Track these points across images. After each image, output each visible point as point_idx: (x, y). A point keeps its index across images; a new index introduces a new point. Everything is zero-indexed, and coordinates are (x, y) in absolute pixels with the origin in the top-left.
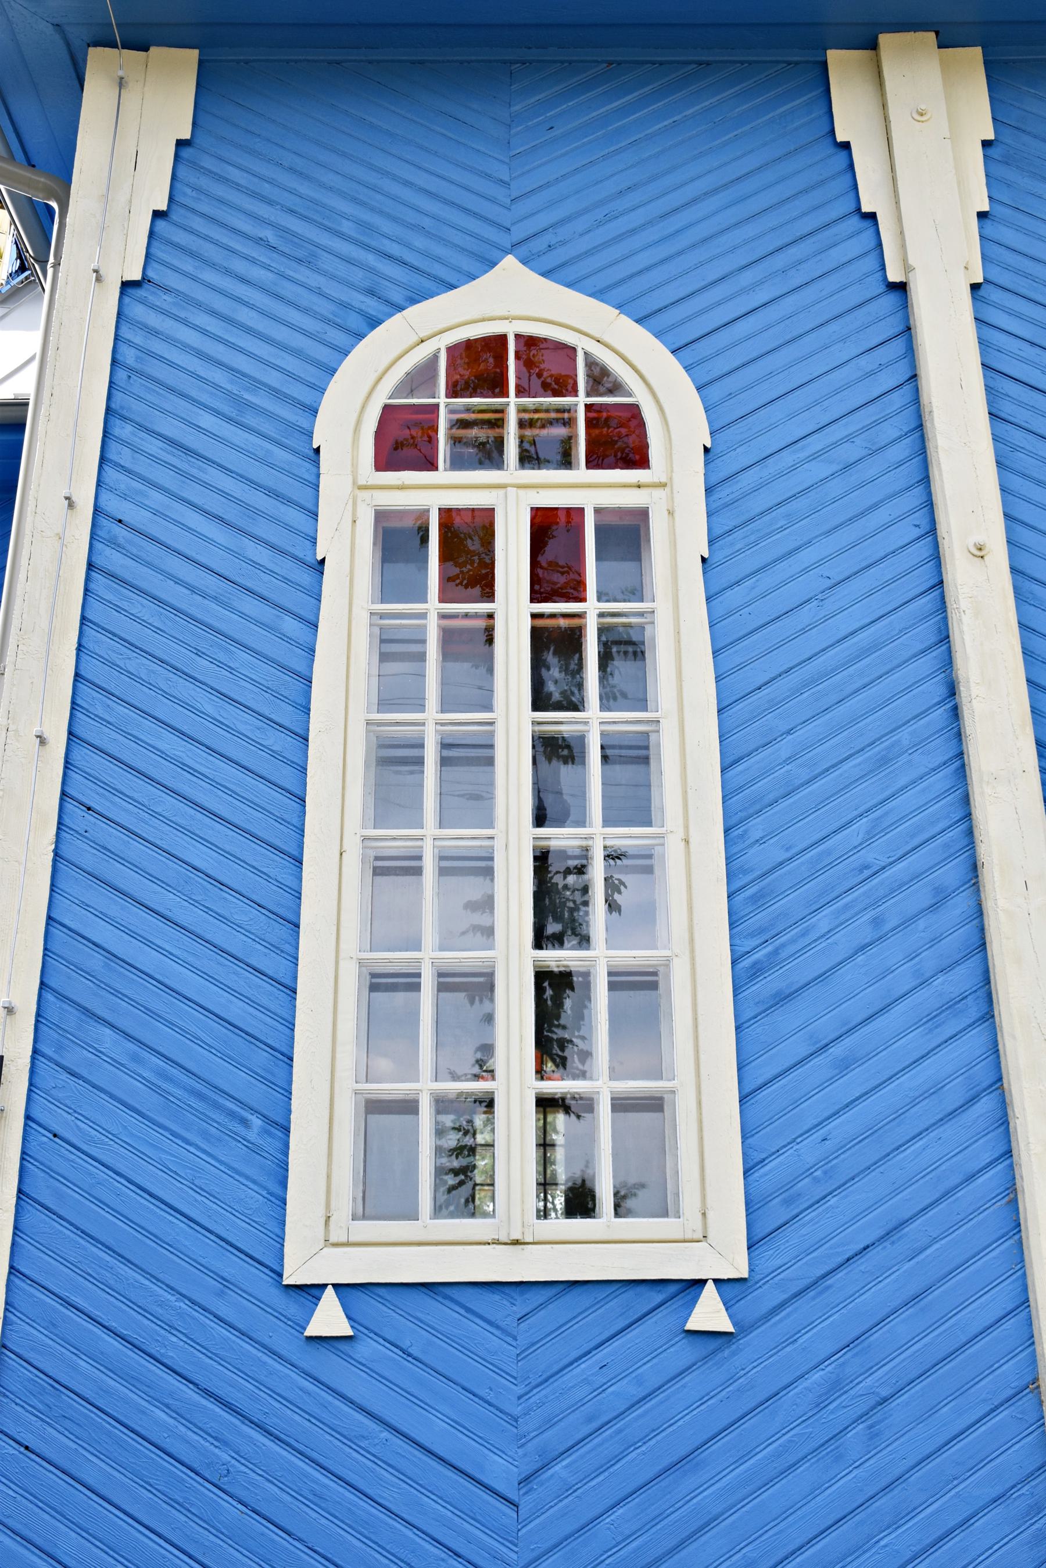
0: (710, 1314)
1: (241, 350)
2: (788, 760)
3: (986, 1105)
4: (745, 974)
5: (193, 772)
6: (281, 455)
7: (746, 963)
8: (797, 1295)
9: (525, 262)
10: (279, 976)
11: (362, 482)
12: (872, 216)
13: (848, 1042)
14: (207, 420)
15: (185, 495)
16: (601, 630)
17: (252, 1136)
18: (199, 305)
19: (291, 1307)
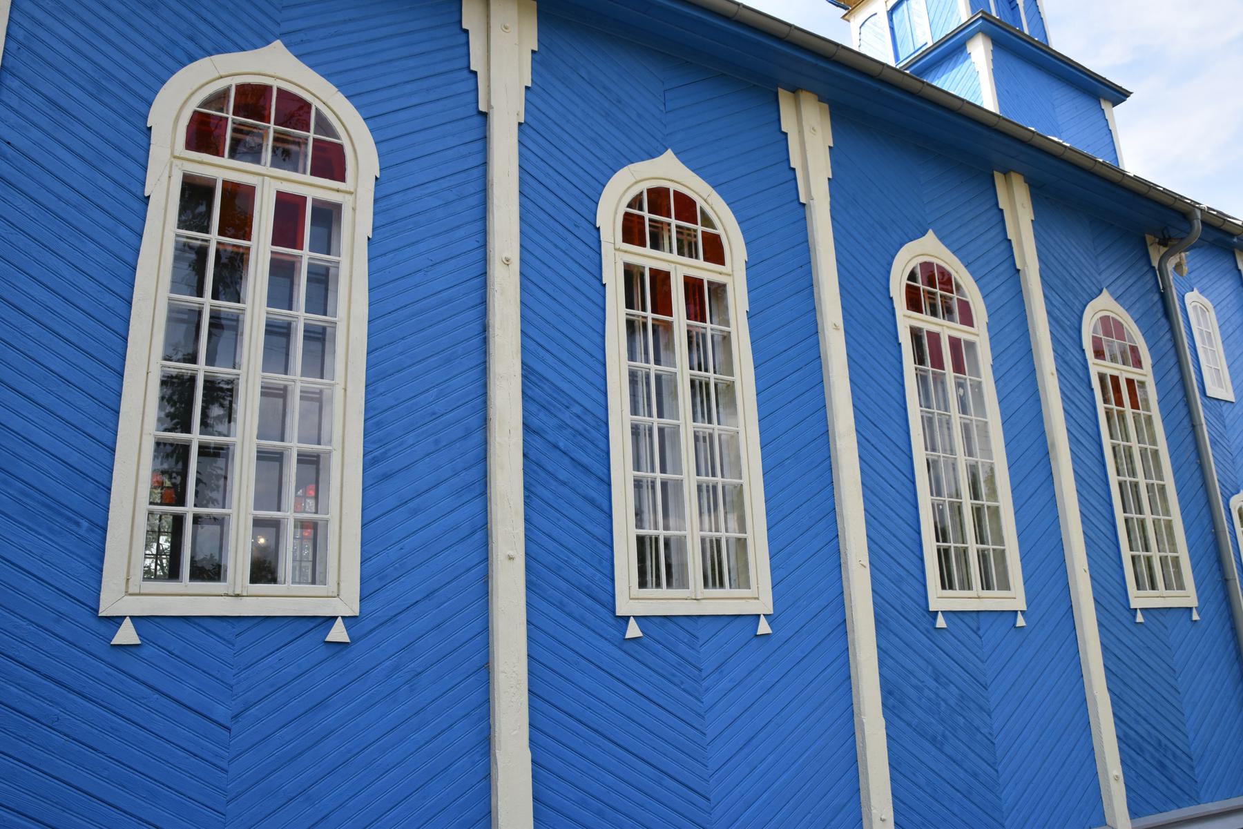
0: (338, 633)
1: (102, 52)
2: (401, 353)
3: (478, 535)
4: (370, 461)
5: (54, 312)
6: (124, 126)
7: (370, 457)
8: (382, 624)
9: (286, 46)
10: (104, 441)
11: (177, 154)
12: (475, 73)
13: (417, 501)
14: (75, 92)
15: (56, 136)
16: (310, 265)
17: (82, 532)
18: (74, 15)
19: (103, 629)
